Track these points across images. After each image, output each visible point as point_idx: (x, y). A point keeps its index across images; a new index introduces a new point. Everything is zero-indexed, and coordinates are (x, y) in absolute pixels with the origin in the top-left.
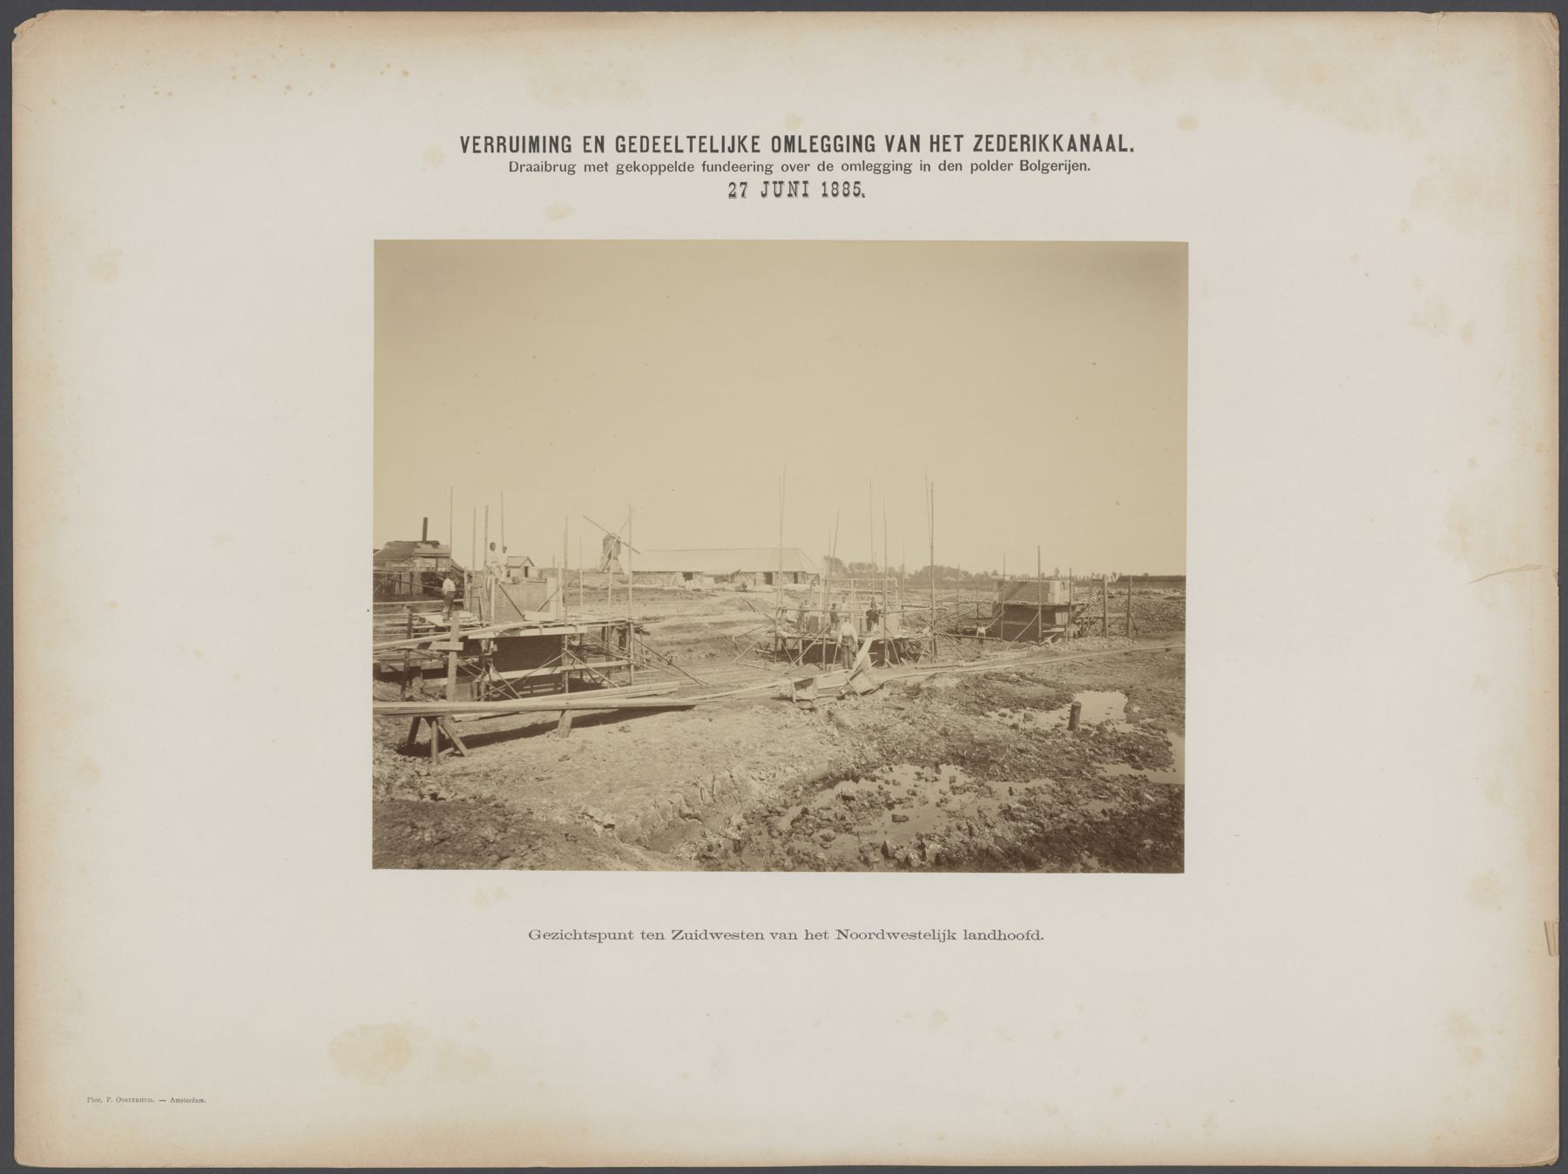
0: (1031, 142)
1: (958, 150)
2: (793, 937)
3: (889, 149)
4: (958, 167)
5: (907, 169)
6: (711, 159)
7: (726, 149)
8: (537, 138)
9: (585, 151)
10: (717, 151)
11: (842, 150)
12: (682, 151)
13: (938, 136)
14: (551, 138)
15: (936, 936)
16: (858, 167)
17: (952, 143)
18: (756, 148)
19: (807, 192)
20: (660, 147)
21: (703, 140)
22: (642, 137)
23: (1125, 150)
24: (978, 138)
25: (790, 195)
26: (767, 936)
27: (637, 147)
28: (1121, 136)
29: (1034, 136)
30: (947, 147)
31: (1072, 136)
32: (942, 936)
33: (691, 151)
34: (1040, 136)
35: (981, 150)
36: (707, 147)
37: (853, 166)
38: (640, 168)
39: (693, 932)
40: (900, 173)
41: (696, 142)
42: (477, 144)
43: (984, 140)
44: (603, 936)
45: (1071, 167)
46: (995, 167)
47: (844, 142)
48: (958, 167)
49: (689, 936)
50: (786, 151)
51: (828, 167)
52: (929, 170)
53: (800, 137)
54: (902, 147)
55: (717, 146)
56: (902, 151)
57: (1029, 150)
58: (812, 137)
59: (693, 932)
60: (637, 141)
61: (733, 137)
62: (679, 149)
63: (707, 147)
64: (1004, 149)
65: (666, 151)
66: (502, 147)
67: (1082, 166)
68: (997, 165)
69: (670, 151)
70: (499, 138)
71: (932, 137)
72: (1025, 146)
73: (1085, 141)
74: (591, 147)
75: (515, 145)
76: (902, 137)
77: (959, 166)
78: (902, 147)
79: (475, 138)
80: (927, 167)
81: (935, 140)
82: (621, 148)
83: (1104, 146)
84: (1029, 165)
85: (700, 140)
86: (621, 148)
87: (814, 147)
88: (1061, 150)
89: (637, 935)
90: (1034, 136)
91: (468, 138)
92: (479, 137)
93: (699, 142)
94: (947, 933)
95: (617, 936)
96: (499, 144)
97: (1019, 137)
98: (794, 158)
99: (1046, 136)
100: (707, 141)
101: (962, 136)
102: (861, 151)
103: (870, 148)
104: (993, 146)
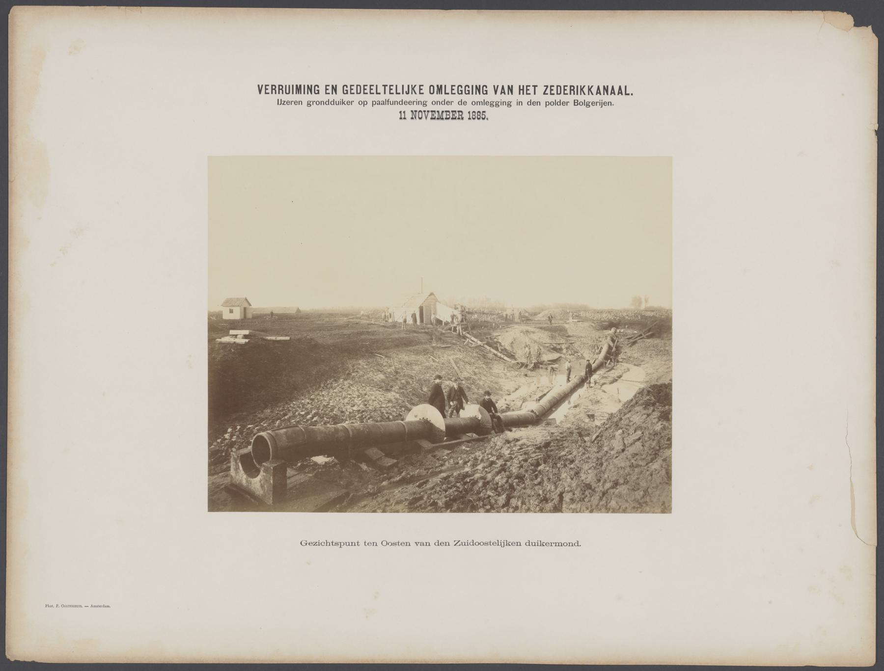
0: (575, 90)
1: (535, 94)
2: (428, 544)
3: (496, 93)
4: (538, 103)
5: (509, 105)
6: (376, 98)
7: (405, 92)
8: (300, 86)
9: (326, 93)
10: (399, 93)
11: (469, 93)
12: (380, 94)
13: (523, 86)
14: (308, 86)
15: (500, 544)
16: (481, 103)
17: (531, 89)
18: (421, 92)
19: (406, 117)
20: (368, 91)
21: (391, 87)
22: (357, 86)
23: (628, 94)
24: (546, 87)
25: (412, 118)
26: (413, 544)
27: (354, 91)
28: (626, 87)
29: (577, 86)
30: (528, 92)
31: (598, 86)
32: (502, 544)
33: (385, 93)
34: (581, 86)
35: (547, 94)
36: (394, 91)
37: (478, 103)
38: (346, 103)
39: (466, 541)
40: (505, 107)
41: (387, 88)
42: (392, 89)
43: (549, 88)
44: (342, 544)
45: (603, 104)
46: (559, 103)
47: (470, 89)
48: (538, 103)
49: (463, 544)
50: (437, 94)
51: (464, 103)
52: (302, 104)
53: (445, 86)
54: (503, 92)
55: (400, 90)
56: (503, 94)
57: (574, 94)
58: (452, 86)
59: (466, 541)
60: (354, 88)
61: (408, 86)
62: (378, 92)
63: (394, 91)
64: (560, 93)
65: (371, 93)
66: (281, 91)
67: (610, 104)
68: (560, 102)
69: (373, 93)
70: (279, 86)
71: (520, 86)
72: (274, 91)
73: (606, 89)
74: (330, 91)
75: (280, 89)
76: (503, 86)
77: (538, 103)
78: (503, 92)
79: (266, 86)
80: (521, 103)
81: (521, 88)
82: (345, 92)
83: (616, 92)
84: (579, 103)
85: (390, 87)
86: (345, 92)
87: (453, 92)
88: (592, 94)
89: (362, 543)
90: (577, 86)
91: (262, 86)
92: (392, 86)
93: (389, 88)
94: (505, 542)
95: (351, 544)
96: (279, 89)
97: (569, 87)
98: (441, 97)
99: (584, 86)
100: (394, 88)
101: (537, 86)
102: (480, 94)
103: (485, 92)
104: (554, 92)
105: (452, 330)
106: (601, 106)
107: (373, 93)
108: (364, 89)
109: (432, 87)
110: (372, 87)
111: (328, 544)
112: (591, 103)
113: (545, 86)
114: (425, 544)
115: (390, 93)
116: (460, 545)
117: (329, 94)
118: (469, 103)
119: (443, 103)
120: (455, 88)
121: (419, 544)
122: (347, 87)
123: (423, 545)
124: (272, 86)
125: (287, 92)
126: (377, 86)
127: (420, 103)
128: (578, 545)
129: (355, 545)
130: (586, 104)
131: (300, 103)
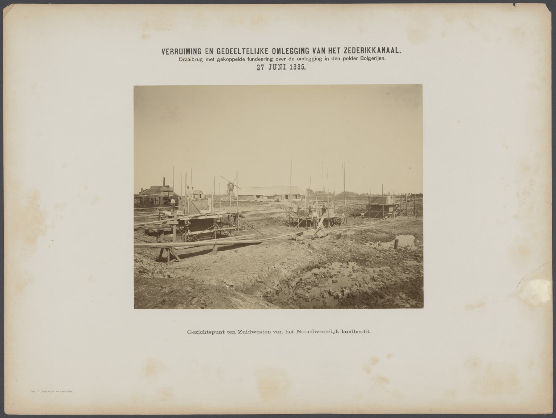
0: (364, 50)
1: (339, 53)
2: (281, 332)
4: (339, 59)
5: (320, 60)
7: (256, 53)
8: (280, 49)
9: (206, 54)
10: (253, 54)
11: (297, 53)
12: (240, 54)
13: (331, 48)
14: (194, 49)
15: (332, 332)
16: (303, 59)
17: (336, 50)
18: (267, 52)
19: (285, 68)
20: (233, 52)
23: (398, 53)
25: (279, 69)
26: (272, 332)
27: (224, 52)
28: (396, 48)
29: (366, 48)
30: (335, 52)
31: (379, 48)
32: (334, 332)
33: (244, 54)
35: (346, 53)
36: (249, 52)
37: (301, 59)
38: (226, 60)
39: (246, 331)
41: (245, 50)
45: (379, 59)
46: (351, 59)
48: (339, 59)
49: (244, 332)
50: (277, 53)
52: (328, 60)
53: (282, 49)
54: (319, 52)
55: (253, 52)
56: (379, 53)
58: (287, 49)
60: (224, 50)
61: (259, 49)
63: (249, 52)
64: (228, 53)
65: (235, 54)
70: (175, 49)
71: (329, 48)
72: (172, 53)
73: (384, 49)
74: (208, 52)
76: (319, 48)
77: (339, 59)
78: (319, 52)
79: (167, 49)
80: (328, 59)
81: (330, 49)
82: (219, 53)
83: (390, 51)
85: (247, 50)
86: (219, 53)
87: (287, 52)
88: (375, 53)
90: (366, 48)
91: (165, 49)
93: (247, 51)
94: (336, 331)
95: (219, 332)
96: (175, 51)
97: (360, 48)
98: (280, 56)
100: (249, 50)
101: (340, 48)
102: (304, 53)
104: (351, 51)
105: (238, 202)
106: (377, 60)
107: (236, 54)
108: (231, 51)
109: (274, 50)
110: (248, 50)
111: (205, 333)
112: (220, 59)
113: (345, 48)
114: (347, 332)
115: (247, 53)
116: (242, 333)
117: (208, 54)
118: (296, 59)
119: (256, 59)
120: (289, 50)
121: (276, 332)
122: (220, 50)
123: (218, 333)
124: (361, 48)
125: (181, 53)
126: (239, 49)
127: (268, 59)
128: (368, 333)
129: (206, 333)
130: (368, 59)
131: (356, 59)
